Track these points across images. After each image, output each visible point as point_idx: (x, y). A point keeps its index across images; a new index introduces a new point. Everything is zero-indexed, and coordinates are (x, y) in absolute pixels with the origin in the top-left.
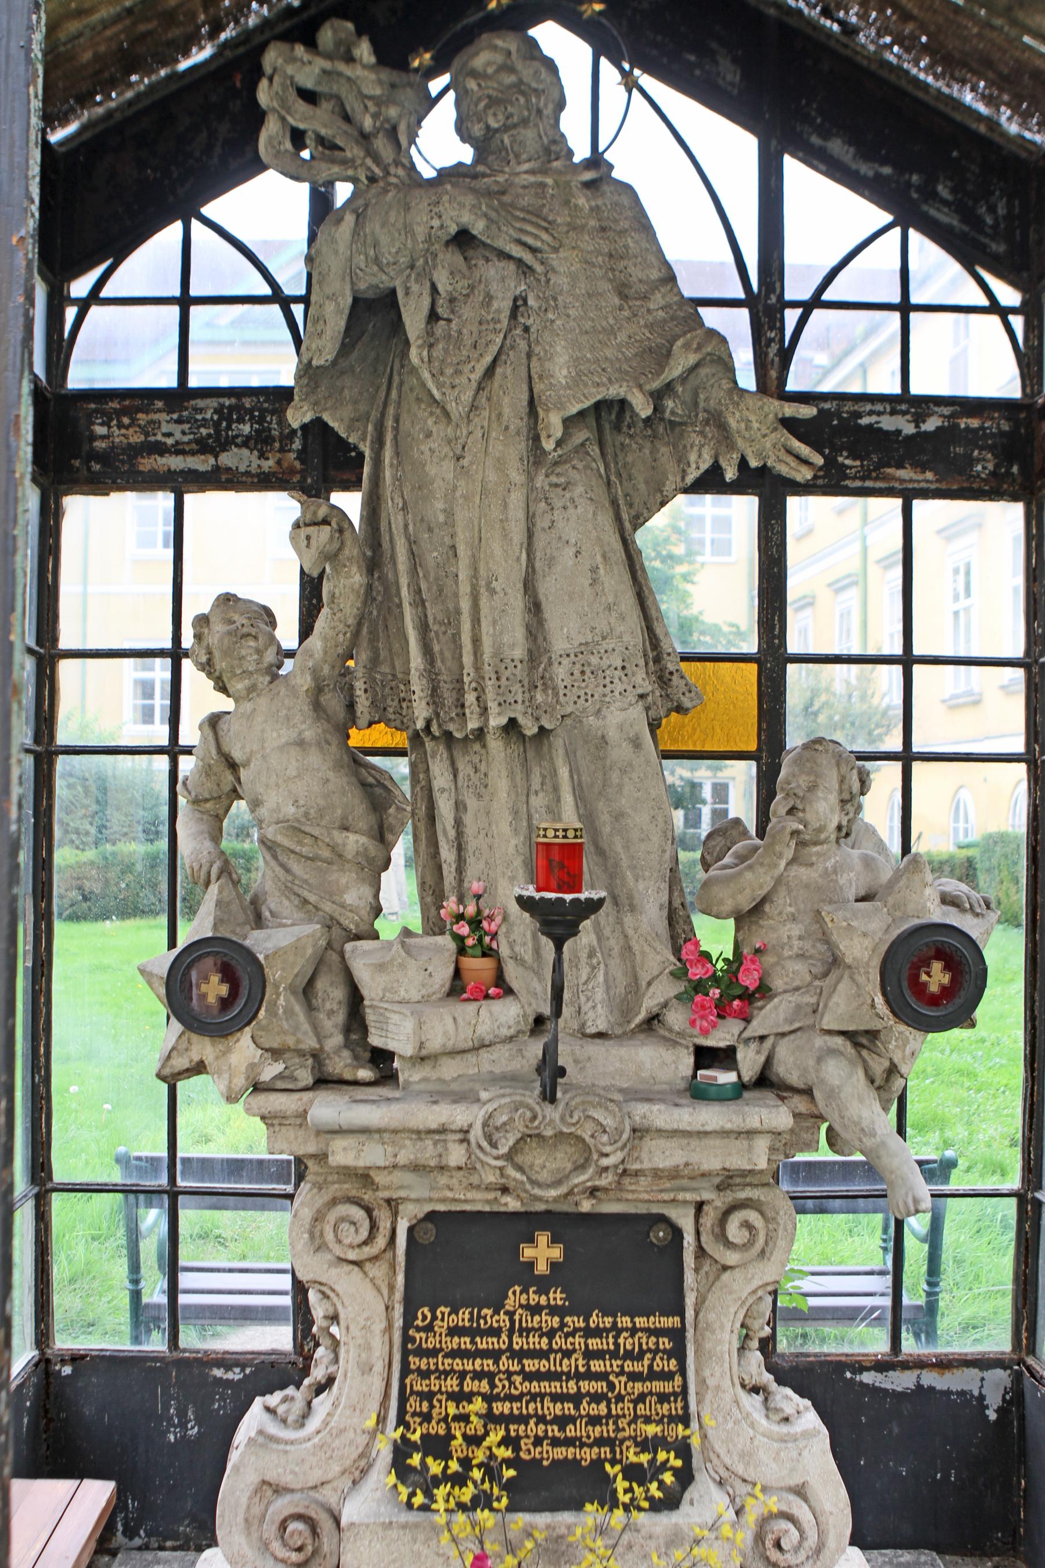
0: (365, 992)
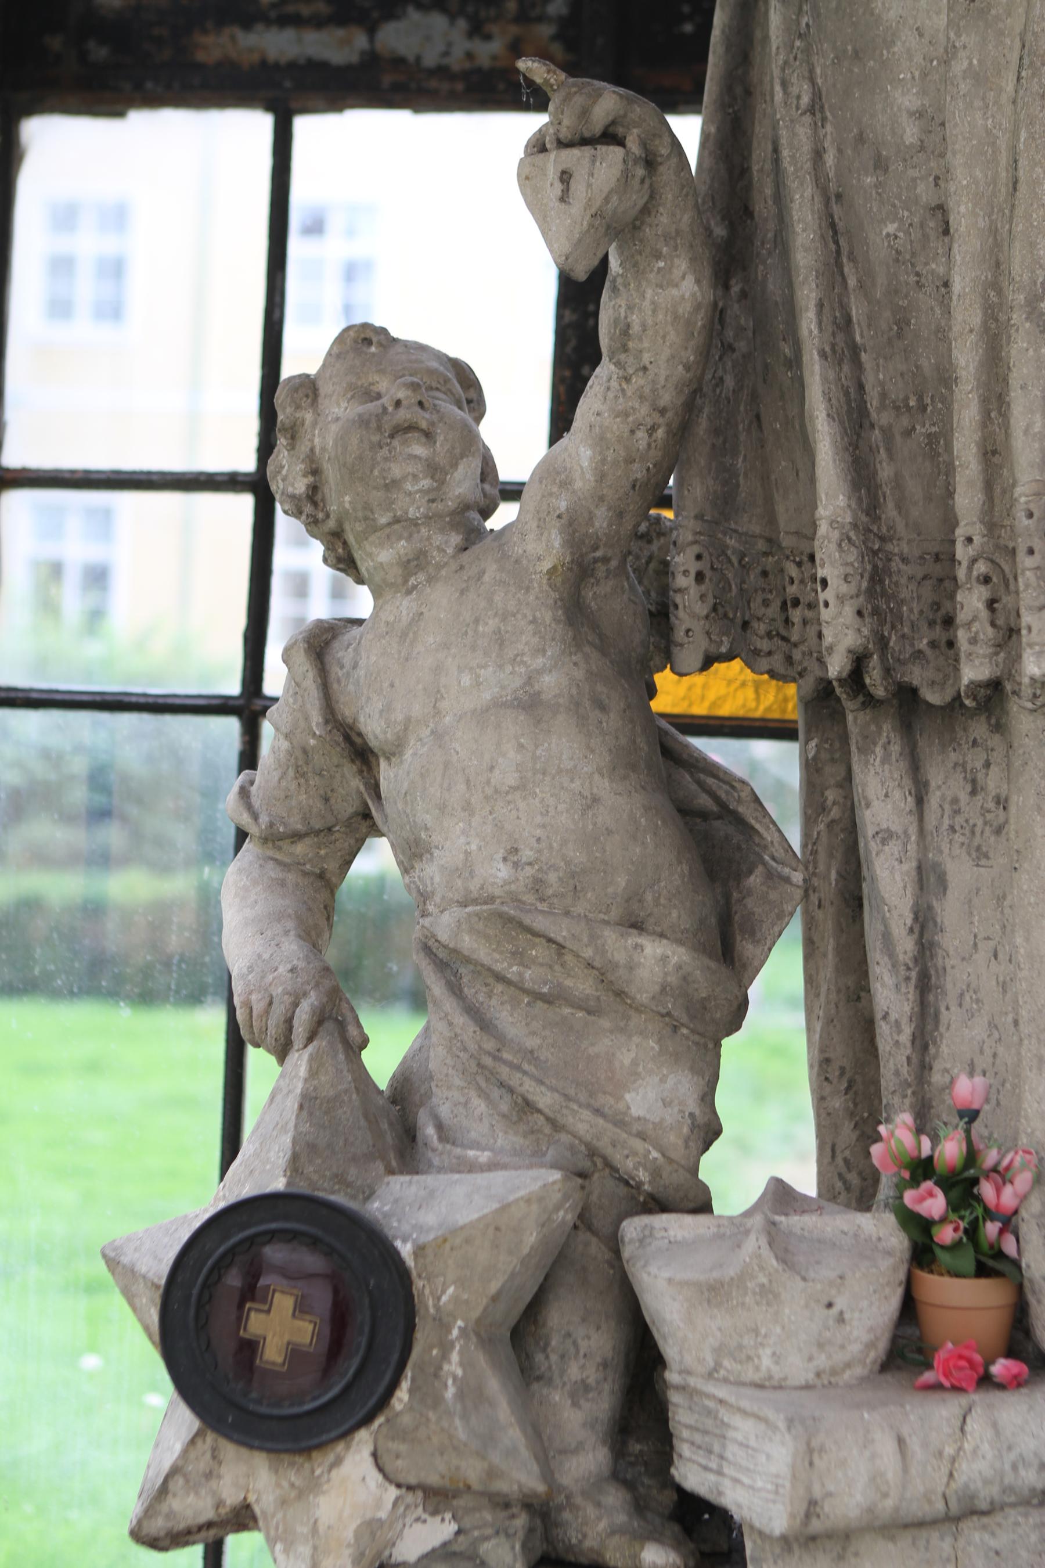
0: (670, 1350)
